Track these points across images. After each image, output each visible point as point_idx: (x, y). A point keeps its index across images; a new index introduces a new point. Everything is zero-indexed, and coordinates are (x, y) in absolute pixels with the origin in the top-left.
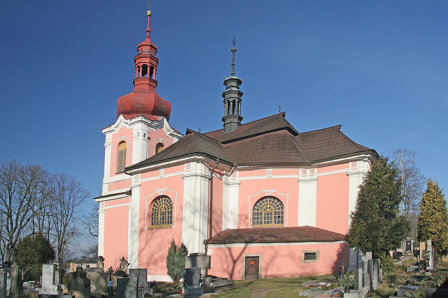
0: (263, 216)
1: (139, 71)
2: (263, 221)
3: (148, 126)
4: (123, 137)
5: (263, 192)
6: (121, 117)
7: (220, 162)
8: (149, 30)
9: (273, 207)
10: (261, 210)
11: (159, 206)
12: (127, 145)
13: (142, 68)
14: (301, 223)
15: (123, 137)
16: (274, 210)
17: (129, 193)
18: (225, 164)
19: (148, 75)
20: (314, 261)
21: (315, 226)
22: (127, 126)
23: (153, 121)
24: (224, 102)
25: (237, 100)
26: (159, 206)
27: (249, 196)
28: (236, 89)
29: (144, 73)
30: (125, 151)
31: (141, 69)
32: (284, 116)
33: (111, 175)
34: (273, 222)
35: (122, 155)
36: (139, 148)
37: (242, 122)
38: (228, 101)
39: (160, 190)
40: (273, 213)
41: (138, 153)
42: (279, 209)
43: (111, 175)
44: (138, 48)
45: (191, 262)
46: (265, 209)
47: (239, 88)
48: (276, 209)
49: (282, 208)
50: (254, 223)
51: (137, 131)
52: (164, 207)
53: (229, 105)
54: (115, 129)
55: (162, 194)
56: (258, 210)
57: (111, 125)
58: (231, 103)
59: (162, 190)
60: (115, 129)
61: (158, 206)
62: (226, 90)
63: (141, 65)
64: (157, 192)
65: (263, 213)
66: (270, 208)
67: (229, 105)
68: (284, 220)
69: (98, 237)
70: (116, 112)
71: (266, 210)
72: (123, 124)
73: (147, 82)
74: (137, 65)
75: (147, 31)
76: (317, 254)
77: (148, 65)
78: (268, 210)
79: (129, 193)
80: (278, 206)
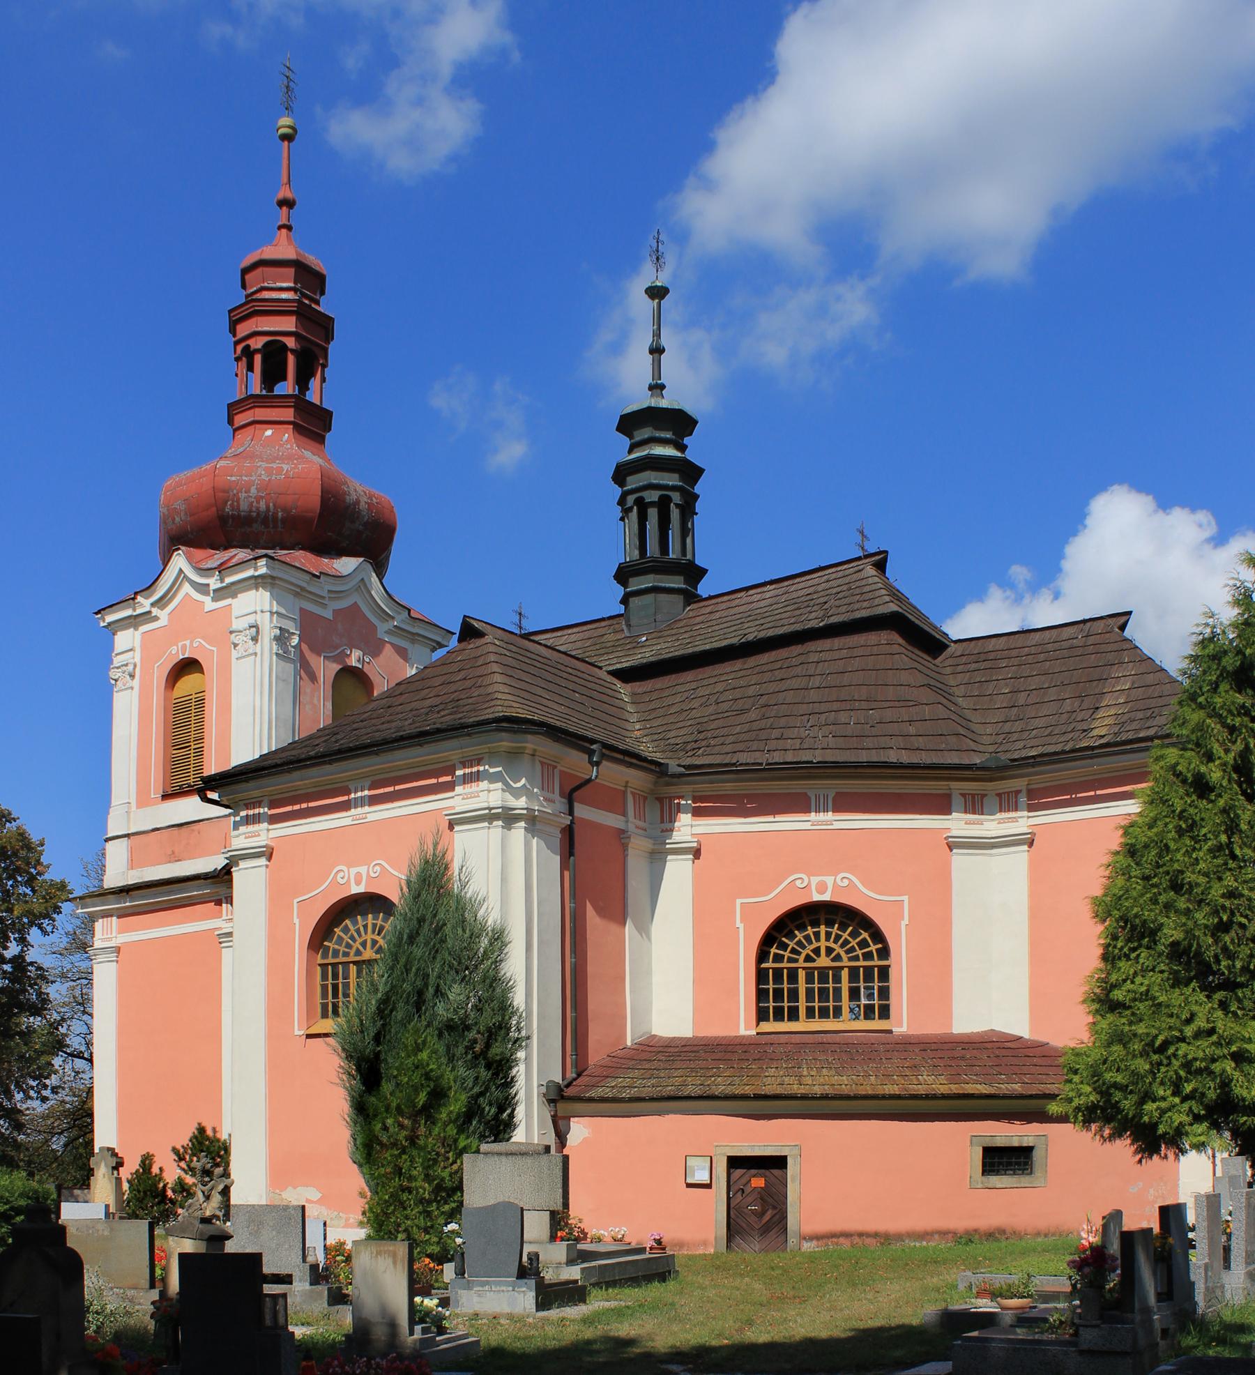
0: (802, 986)
1: (250, 368)
2: (802, 1004)
3: (296, 594)
4: (188, 643)
5: (798, 883)
6: (179, 561)
7: (603, 756)
8: (289, 195)
9: (842, 946)
10: (790, 960)
11: (352, 938)
12: (209, 682)
13: (264, 361)
14: (967, 1020)
15: (188, 643)
16: (850, 959)
17: (223, 877)
18: (631, 765)
19: (287, 387)
20: (1024, 1180)
21: (1032, 1030)
22: (208, 603)
23: (318, 577)
24: (622, 502)
25: (676, 497)
26: (352, 938)
27: (739, 901)
28: (669, 451)
29: (273, 374)
30: (201, 702)
31: (258, 359)
32: (881, 566)
33: (143, 801)
34: (845, 1010)
35: (184, 725)
36: (257, 716)
37: (704, 589)
38: (640, 503)
39: (353, 871)
40: (845, 974)
41: (248, 721)
42: (868, 956)
43: (143, 801)
44: (245, 271)
45: (708, 147)
46: (808, 955)
47: (682, 448)
48: (856, 958)
49: (884, 953)
50: (762, 1015)
51: (251, 620)
52: (374, 942)
53: (642, 519)
54: (155, 611)
55: (361, 889)
56: (778, 958)
57: (136, 594)
58: (653, 514)
59: (363, 870)
60: (155, 611)
61: (342, 949)
62: (630, 451)
63: (257, 343)
64: (342, 882)
65: (802, 975)
66: (829, 951)
67: (642, 519)
68: (893, 1001)
69: (91, 1061)
70: (153, 538)
71: (814, 961)
72: (187, 588)
73: (288, 414)
74: (243, 345)
75: (280, 228)
76: (1036, 1154)
77: (291, 342)
78: (823, 961)
79: (223, 877)
80: (863, 944)
